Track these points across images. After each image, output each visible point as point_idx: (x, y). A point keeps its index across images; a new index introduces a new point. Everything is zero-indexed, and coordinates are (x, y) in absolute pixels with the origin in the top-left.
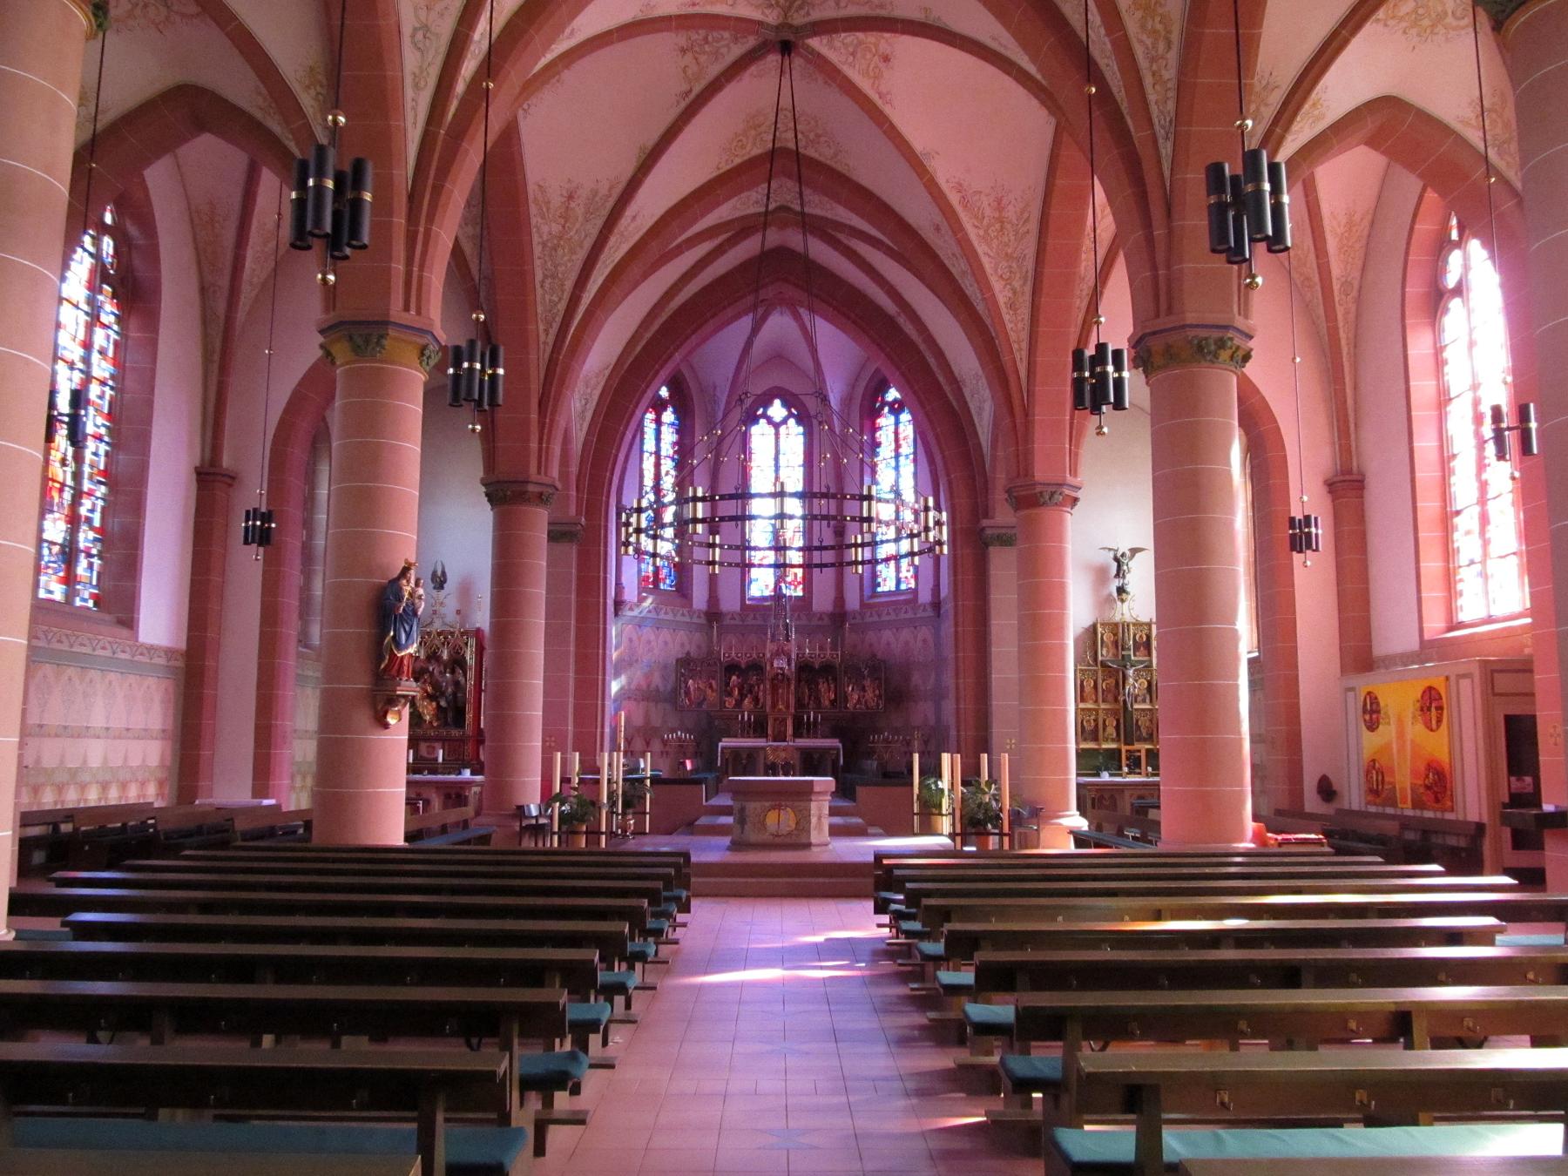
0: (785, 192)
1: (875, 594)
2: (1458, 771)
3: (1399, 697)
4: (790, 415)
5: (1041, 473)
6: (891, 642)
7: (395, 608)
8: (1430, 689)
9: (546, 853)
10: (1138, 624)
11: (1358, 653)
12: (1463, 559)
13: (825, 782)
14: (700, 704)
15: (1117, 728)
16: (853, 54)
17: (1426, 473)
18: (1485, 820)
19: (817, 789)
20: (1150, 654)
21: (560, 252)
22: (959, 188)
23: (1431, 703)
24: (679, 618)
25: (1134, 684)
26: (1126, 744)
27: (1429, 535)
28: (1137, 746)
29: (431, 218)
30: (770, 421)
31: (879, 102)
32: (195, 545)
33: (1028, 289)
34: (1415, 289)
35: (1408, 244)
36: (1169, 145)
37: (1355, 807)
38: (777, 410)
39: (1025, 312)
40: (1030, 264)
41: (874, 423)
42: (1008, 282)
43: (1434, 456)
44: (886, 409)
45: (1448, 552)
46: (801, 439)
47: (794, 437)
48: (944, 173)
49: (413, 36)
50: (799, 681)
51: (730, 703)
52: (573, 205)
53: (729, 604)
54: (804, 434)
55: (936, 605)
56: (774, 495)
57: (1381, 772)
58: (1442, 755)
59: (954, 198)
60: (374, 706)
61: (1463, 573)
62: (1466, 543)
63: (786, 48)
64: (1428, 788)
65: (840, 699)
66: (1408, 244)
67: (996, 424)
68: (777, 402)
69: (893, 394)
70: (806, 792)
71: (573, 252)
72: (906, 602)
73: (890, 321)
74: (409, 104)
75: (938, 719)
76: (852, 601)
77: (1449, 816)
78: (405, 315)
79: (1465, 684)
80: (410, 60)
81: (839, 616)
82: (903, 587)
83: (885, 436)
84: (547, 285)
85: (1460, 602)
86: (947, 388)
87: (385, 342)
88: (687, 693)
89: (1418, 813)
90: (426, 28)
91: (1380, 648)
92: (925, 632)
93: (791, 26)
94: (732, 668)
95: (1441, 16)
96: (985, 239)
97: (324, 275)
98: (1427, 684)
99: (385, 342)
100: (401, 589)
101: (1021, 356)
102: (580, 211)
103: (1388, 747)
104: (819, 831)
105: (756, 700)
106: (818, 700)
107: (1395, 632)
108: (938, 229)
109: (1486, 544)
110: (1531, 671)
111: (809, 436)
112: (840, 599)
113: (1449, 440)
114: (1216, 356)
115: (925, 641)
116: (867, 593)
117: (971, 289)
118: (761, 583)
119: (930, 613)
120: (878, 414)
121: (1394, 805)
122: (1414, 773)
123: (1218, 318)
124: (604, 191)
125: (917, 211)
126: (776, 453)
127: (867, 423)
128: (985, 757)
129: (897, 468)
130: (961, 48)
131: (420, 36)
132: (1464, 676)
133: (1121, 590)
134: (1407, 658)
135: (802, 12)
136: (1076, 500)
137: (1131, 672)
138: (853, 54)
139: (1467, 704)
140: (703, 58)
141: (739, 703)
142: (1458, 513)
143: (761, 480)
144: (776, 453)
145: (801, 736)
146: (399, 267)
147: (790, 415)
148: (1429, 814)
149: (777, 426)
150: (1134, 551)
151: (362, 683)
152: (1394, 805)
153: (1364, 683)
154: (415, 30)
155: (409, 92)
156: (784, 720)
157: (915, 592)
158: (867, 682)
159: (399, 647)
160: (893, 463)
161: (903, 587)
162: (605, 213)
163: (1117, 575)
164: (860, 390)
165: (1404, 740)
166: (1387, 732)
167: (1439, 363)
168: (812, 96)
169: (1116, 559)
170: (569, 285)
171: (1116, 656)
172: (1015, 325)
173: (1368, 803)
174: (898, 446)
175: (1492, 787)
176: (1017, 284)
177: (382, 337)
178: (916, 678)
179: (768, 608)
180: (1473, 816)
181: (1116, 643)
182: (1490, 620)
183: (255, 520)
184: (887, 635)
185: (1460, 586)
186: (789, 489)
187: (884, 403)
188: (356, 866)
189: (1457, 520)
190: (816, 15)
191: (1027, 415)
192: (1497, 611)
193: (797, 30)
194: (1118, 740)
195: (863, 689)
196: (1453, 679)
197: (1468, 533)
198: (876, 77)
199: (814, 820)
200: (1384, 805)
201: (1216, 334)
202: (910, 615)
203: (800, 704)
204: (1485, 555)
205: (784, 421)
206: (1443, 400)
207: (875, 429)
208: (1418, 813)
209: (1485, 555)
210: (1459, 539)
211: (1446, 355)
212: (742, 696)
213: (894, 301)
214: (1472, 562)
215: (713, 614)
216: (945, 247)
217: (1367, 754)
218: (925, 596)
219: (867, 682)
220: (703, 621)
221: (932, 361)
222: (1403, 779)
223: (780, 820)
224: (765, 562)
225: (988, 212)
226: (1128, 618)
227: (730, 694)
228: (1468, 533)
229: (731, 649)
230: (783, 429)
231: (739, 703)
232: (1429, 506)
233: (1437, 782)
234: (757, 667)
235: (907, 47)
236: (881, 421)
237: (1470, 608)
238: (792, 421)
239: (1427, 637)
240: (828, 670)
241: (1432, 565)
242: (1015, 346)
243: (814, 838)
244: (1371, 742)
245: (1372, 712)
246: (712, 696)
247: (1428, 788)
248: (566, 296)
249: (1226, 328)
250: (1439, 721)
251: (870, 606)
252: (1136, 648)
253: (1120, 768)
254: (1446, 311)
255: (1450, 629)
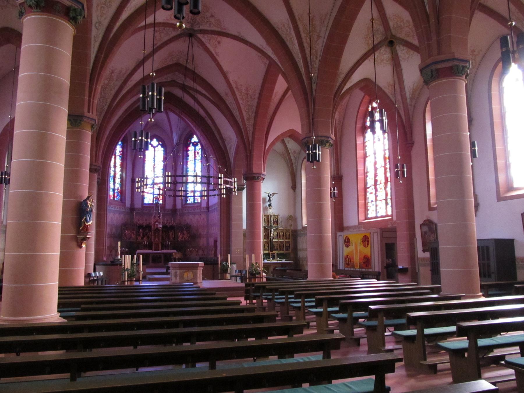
0: (180, 78)
1: (186, 204)
2: (373, 258)
3: (356, 238)
4: (159, 144)
5: (255, 170)
6: (193, 220)
7: (86, 209)
8: (365, 236)
9: (94, 287)
10: (274, 216)
11: (339, 225)
12: (369, 200)
13: (201, 264)
14: (129, 239)
15: (268, 246)
16: (210, 40)
17: (361, 176)
18: (380, 271)
19: (200, 266)
20: (278, 225)
21: (107, 90)
22: (236, 83)
23: (366, 240)
24: (116, 209)
25: (273, 233)
26: (271, 251)
27: (361, 193)
28: (274, 252)
29: (96, 84)
30: (152, 146)
31: (215, 55)
32: (342, 215)
33: (253, 115)
34: (359, 125)
35: (358, 113)
36: (315, 85)
37: (341, 268)
38: (155, 142)
39: (252, 122)
40: (254, 108)
41: (187, 149)
42: (248, 112)
43: (362, 172)
44: (191, 145)
45: (366, 199)
46: (163, 152)
47: (160, 152)
48: (232, 78)
49: (95, 25)
50: (162, 232)
51: (139, 238)
52: (113, 75)
53: (138, 205)
54: (164, 151)
55: (208, 208)
56: (194, 176)
57: (350, 259)
58: (369, 254)
59: (234, 86)
60: (77, 241)
61: (369, 204)
62: (371, 197)
63: (191, 36)
64: (364, 263)
65: (176, 237)
66: (358, 113)
67: (237, 152)
68: (155, 140)
69: (195, 139)
70: (196, 267)
71: (111, 90)
72: (197, 207)
73: (202, 119)
74: (92, 46)
75: (208, 244)
76: (179, 206)
77: (370, 270)
78: (88, 114)
79: (375, 235)
80: (94, 32)
81: (174, 211)
82: (196, 201)
83: (191, 153)
84: (101, 100)
85: (368, 212)
86: (220, 141)
87: (82, 122)
88: (125, 235)
89: (361, 270)
90: (100, 22)
91: (345, 224)
92: (204, 216)
93: (193, 29)
94: (140, 227)
95: (383, 60)
96: (242, 99)
97: (151, 119)
98: (363, 235)
99: (82, 122)
100: (87, 203)
101: (250, 135)
102: (115, 77)
103: (352, 252)
104: (199, 279)
105: (148, 237)
106: (169, 239)
107: (351, 219)
108: (227, 94)
109: (376, 196)
110: (396, 231)
111: (166, 153)
112: (175, 205)
113: (367, 168)
114: (325, 145)
115: (203, 219)
116: (184, 203)
117: (236, 113)
118: (148, 199)
119: (205, 210)
120: (189, 146)
121: (354, 267)
122: (360, 259)
123: (326, 134)
124: (124, 72)
125: (220, 87)
126: (154, 158)
127: (185, 149)
128: (229, 255)
129: (195, 163)
130: (231, 38)
131: (97, 25)
132: (375, 233)
133: (270, 205)
134: (354, 227)
135: (198, 26)
136: (264, 179)
137: (272, 230)
138: (210, 40)
139: (376, 240)
140: (162, 35)
141: (143, 238)
142: (369, 188)
143: (191, 173)
144: (154, 158)
145: (163, 249)
146: (87, 98)
147: (159, 144)
148: (364, 270)
149: (154, 147)
150: (274, 194)
151: (73, 233)
152: (354, 267)
153: (344, 234)
154: (97, 23)
155: (92, 43)
156: (158, 244)
157: (201, 203)
158: (185, 232)
159: (87, 222)
160: (193, 162)
161: (196, 201)
162: (123, 79)
163: (269, 201)
164: (183, 138)
165: (356, 250)
166: (352, 248)
167: (364, 146)
168: (198, 51)
169: (268, 196)
170: (109, 101)
171: (268, 225)
172: (249, 125)
173: (345, 267)
174: (195, 157)
175: (382, 261)
176: (250, 113)
177: (81, 121)
178: (200, 230)
179: (153, 207)
180: (377, 270)
181: (268, 221)
182: (377, 217)
183: (5, 175)
184: (191, 217)
185: (368, 208)
186: (198, 174)
187: (191, 142)
188: (73, 292)
189: (368, 190)
190: (202, 28)
191: (251, 153)
192: (379, 215)
193: (195, 31)
194: (268, 250)
195: (184, 234)
196: (372, 234)
197: (371, 193)
198: (215, 47)
199: (198, 275)
200: (350, 268)
201: (326, 139)
202: (199, 211)
203: (163, 239)
204: (376, 200)
205: (157, 146)
206: (365, 157)
207: (187, 150)
208: (361, 270)
209: (376, 200)
210: (368, 195)
211: (366, 144)
212: (144, 236)
213: (205, 112)
214: (372, 201)
215: (132, 209)
216: (229, 100)
217: (345, 254)
218: (204, 205)
219: (185, 232)
220: (129, 211)
221: (216, 133)
222: (357, 260)
223: (188, 275)
224: (149, 192)
225: (243, 91)
226: (272, 214)
227: (139, 235)
228: (371, 193)
229: (138, 220)
230: (156, 148)
231: (143, 238)
232: (361, 185)
233: (367, 261)
234: (149, 227)
235: (225, 40)
236: (190, 148)
237: (371, 214)
238: (160, 146)
239: (360, 221)
240: (172, 228)
241: (361, 202)
242: (248, 132)
243: (198, 281)
244: (347, 251)
245: (347, 242)
246: (133, 236)
247: (364, 263)
248: (108, 104)
249: (328, 137)
250: (368, 245)
251: (186, 207)
252: (274, 223)
253: (269, 259)
254: (366, 132)
255: (366, 219)
